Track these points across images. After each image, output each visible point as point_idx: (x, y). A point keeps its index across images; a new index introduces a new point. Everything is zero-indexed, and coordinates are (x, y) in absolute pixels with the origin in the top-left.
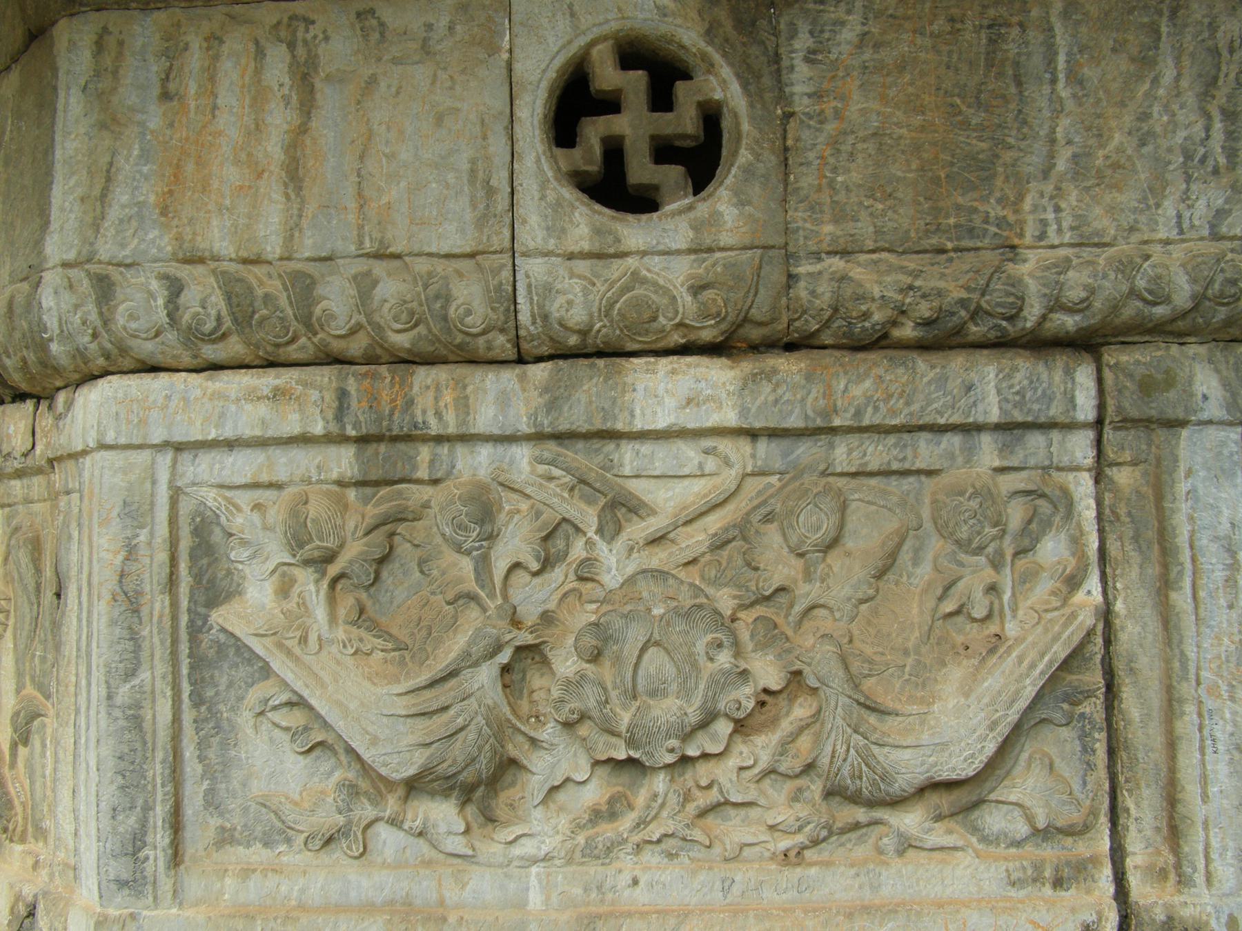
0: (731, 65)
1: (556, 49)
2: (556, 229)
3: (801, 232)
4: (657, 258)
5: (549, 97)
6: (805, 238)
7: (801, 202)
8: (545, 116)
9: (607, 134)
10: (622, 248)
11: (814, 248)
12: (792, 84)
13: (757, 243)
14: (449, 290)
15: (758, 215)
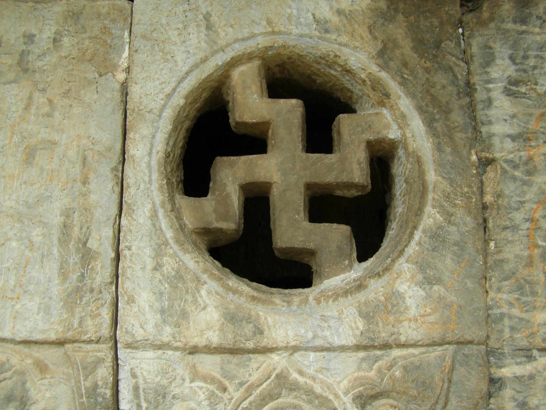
0: (412, 95)
1: (185, 69)
2: (174, 314)
3: (506, 321)
4: (312, 355)
5: (175, 128)
6: (512, 329)
7: (506, 279)
8: (167, 155)
9: (249, 179)
10: (265, 342)
11: (524, 343)
12: (490, 123)
13: (449, 337)
14: (26, 390)
15: (452, 298)
